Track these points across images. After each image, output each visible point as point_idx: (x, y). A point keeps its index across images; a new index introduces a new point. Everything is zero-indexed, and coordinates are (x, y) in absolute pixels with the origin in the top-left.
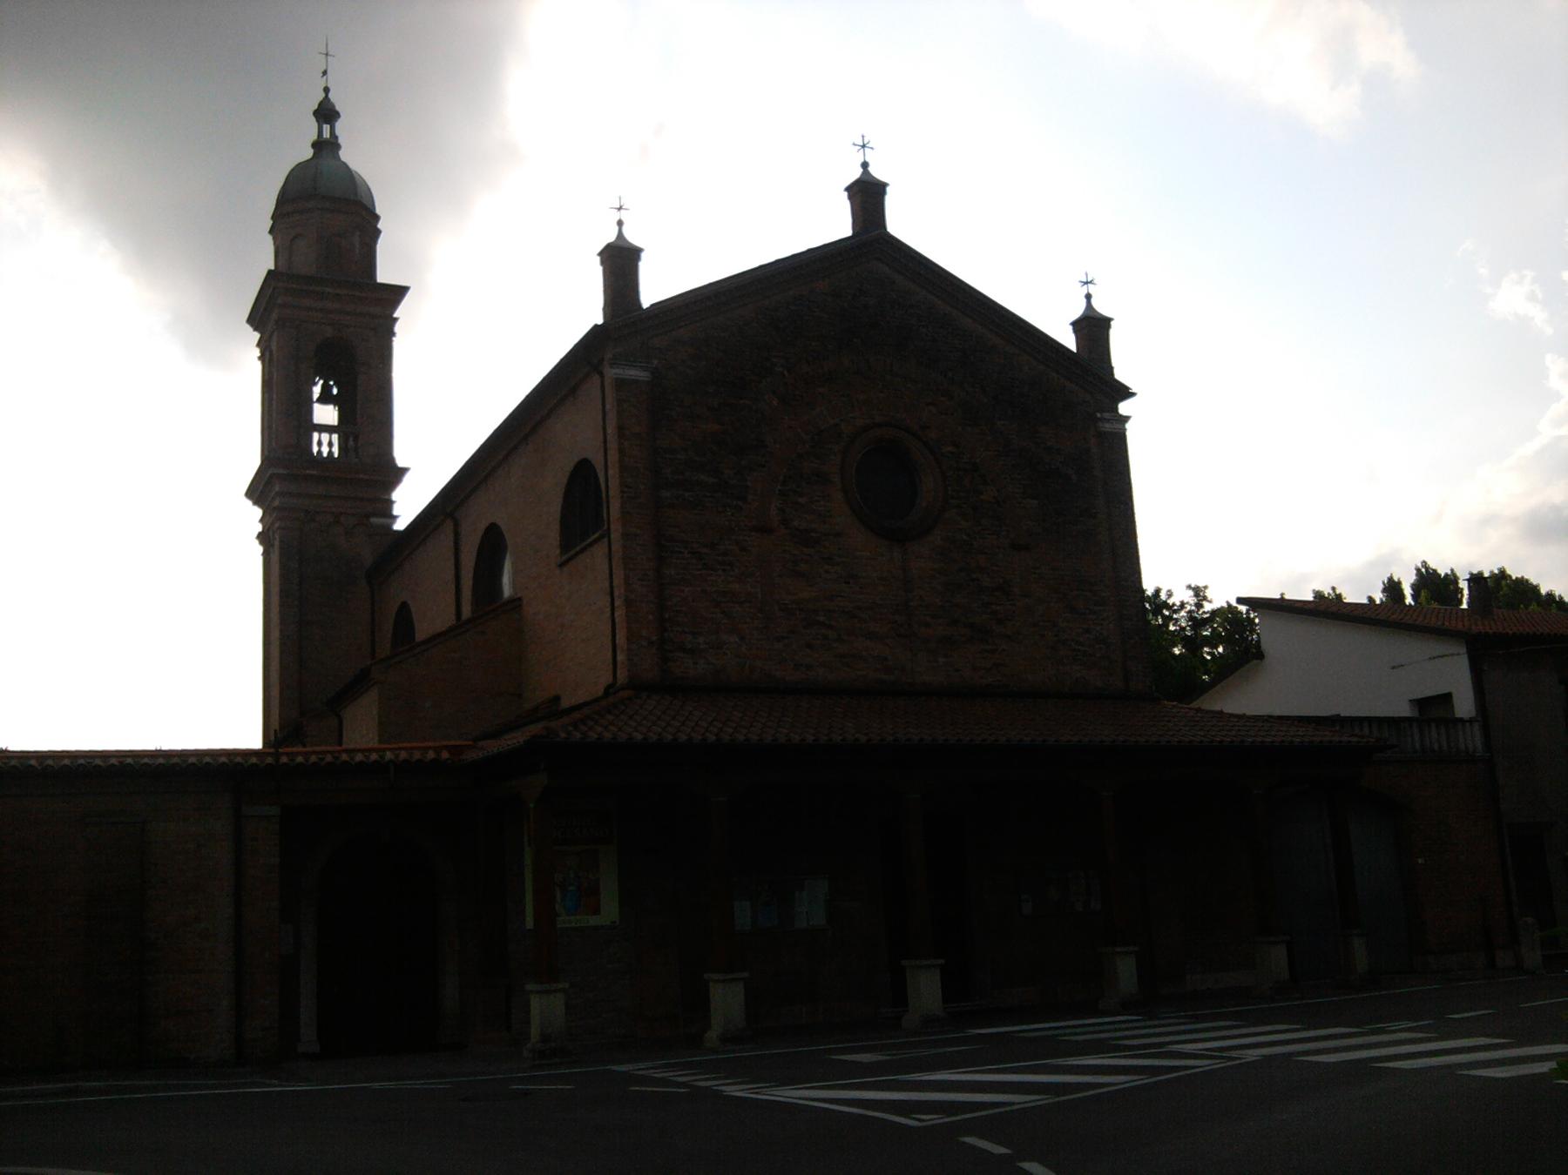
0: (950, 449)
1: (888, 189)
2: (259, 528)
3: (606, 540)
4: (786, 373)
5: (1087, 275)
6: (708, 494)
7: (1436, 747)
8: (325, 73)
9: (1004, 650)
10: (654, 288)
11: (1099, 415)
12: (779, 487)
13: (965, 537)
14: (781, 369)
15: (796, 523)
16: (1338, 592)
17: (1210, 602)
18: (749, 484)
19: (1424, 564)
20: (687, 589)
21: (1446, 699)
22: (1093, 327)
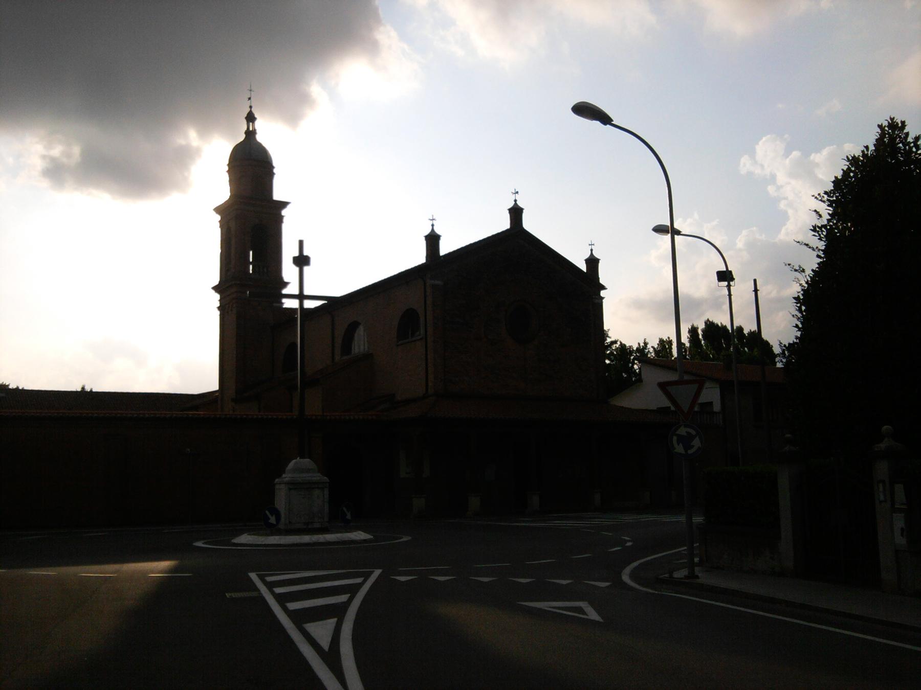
1: (524, 211)
2: (218, 305)
8: (250, 99)
10: (445, 249)
11: (594, 297)
16: (670, 339)
17: (610, 338)
19: (708, 320)
21: (711, 404)
22: (593, 262)
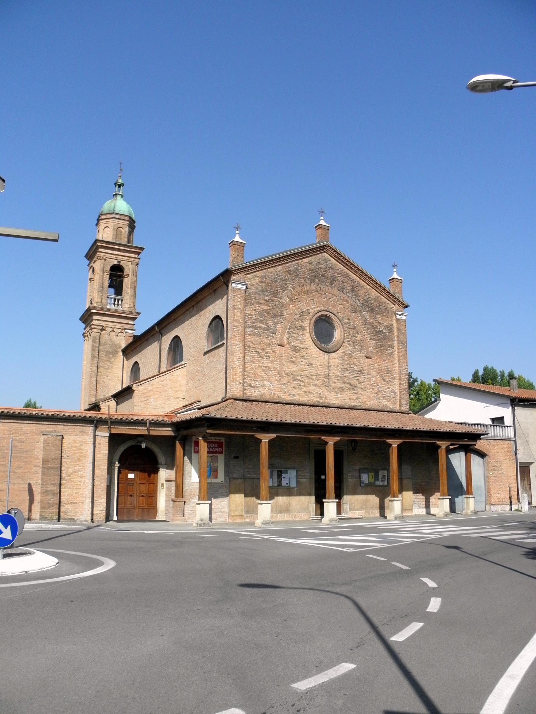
0: (347, 321)
3: (224, 348)
4: (292, 289)
5: (395, 263)
6: (263, 331)
7: (498, 435)
9: (360, 393)
12: (287, 330)
13: (350, 352)
14: (290, 288)
15: (292, 344)
18: (277, 328)
20: (253, 365)
